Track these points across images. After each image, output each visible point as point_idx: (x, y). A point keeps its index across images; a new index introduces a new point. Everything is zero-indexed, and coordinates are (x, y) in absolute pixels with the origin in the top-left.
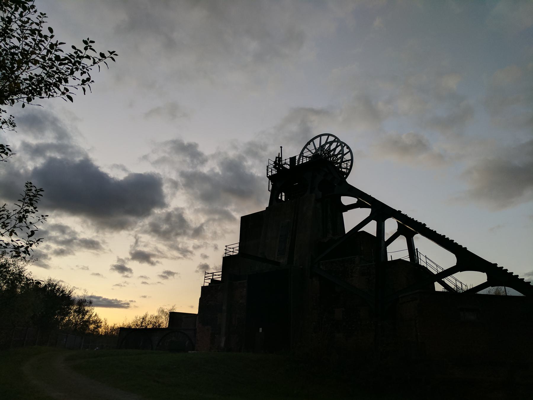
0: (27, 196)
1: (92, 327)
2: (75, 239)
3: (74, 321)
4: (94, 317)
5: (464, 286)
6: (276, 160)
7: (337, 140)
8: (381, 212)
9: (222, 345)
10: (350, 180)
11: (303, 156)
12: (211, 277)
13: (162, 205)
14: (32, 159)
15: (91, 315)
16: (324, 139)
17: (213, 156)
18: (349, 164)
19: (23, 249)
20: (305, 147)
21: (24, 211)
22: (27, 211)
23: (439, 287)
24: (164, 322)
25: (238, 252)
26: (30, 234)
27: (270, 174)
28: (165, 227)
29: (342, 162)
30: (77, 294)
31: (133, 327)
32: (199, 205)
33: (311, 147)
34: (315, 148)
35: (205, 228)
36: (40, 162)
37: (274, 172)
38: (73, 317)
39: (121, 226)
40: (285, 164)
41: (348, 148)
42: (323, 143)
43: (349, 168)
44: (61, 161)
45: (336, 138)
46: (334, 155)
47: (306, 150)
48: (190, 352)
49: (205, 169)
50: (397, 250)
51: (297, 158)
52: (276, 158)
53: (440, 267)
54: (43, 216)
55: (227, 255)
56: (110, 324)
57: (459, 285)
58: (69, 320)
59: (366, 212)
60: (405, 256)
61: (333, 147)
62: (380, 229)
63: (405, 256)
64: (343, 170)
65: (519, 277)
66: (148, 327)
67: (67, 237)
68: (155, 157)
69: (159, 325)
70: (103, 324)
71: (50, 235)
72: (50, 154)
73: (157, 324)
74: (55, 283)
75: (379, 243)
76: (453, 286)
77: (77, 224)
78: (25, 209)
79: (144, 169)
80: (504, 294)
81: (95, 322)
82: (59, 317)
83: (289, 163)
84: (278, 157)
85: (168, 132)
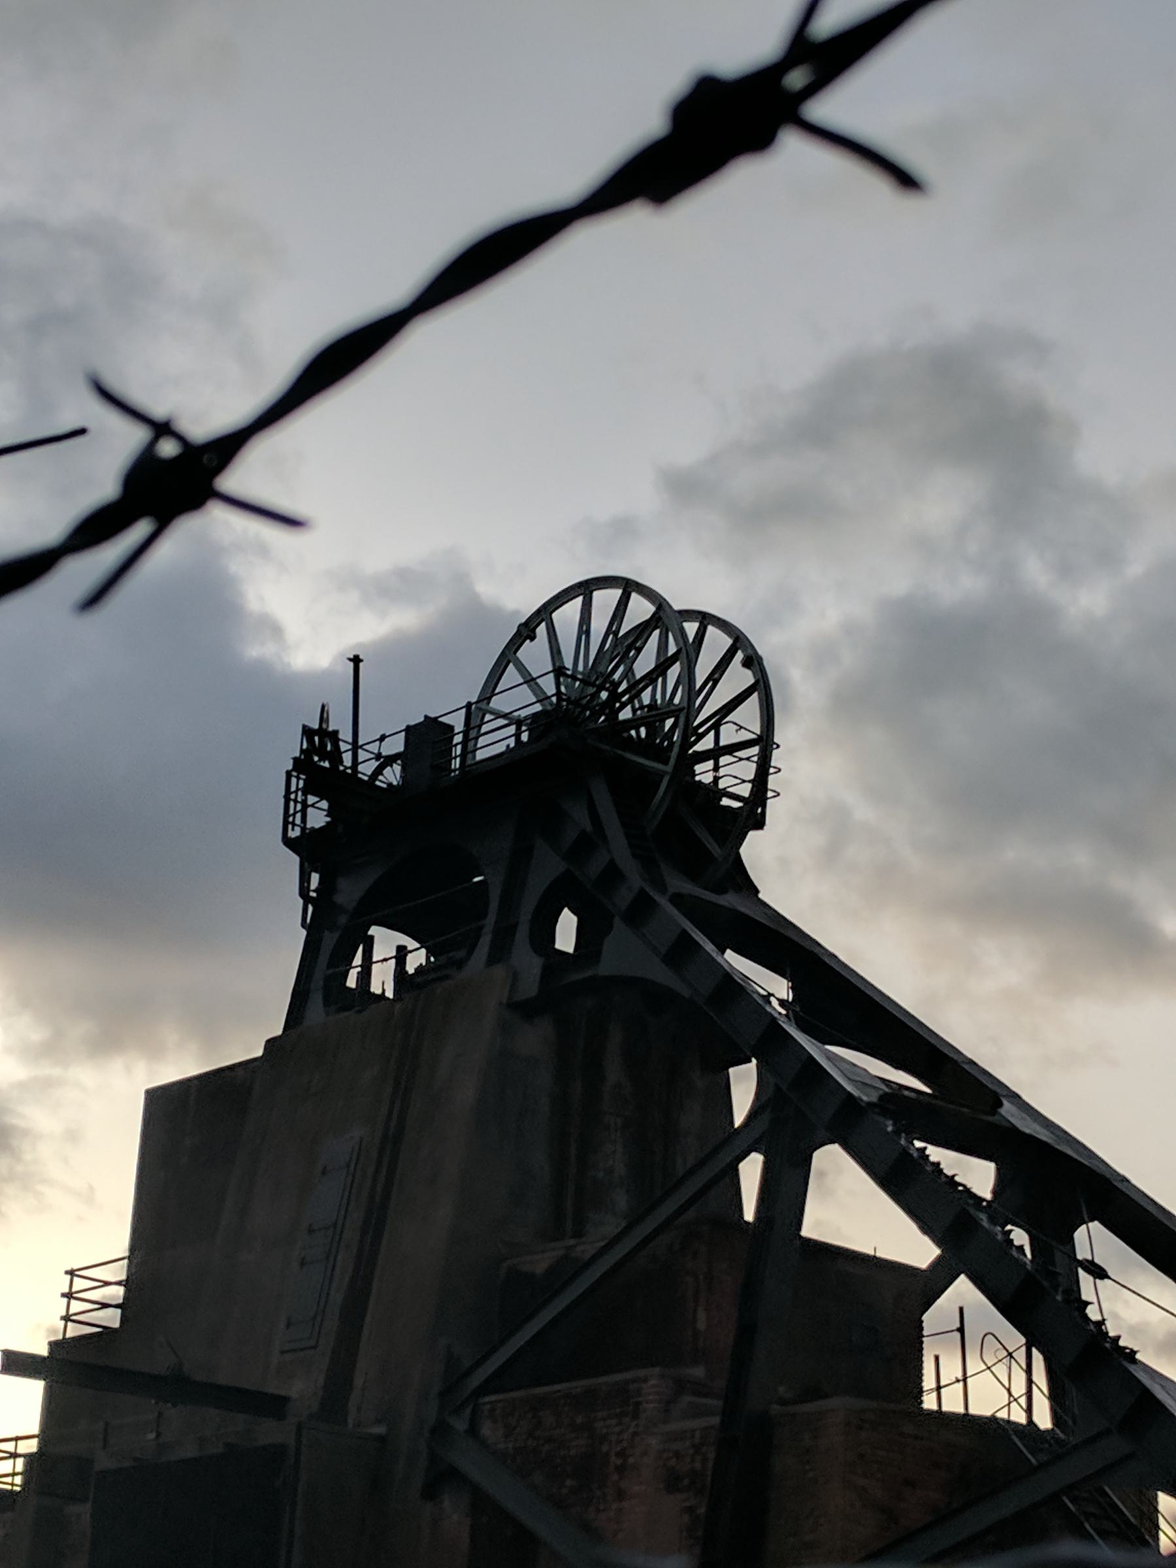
18: (749, 770)
27: (294, 833)
33: (536, 654)
47: (511, 675)
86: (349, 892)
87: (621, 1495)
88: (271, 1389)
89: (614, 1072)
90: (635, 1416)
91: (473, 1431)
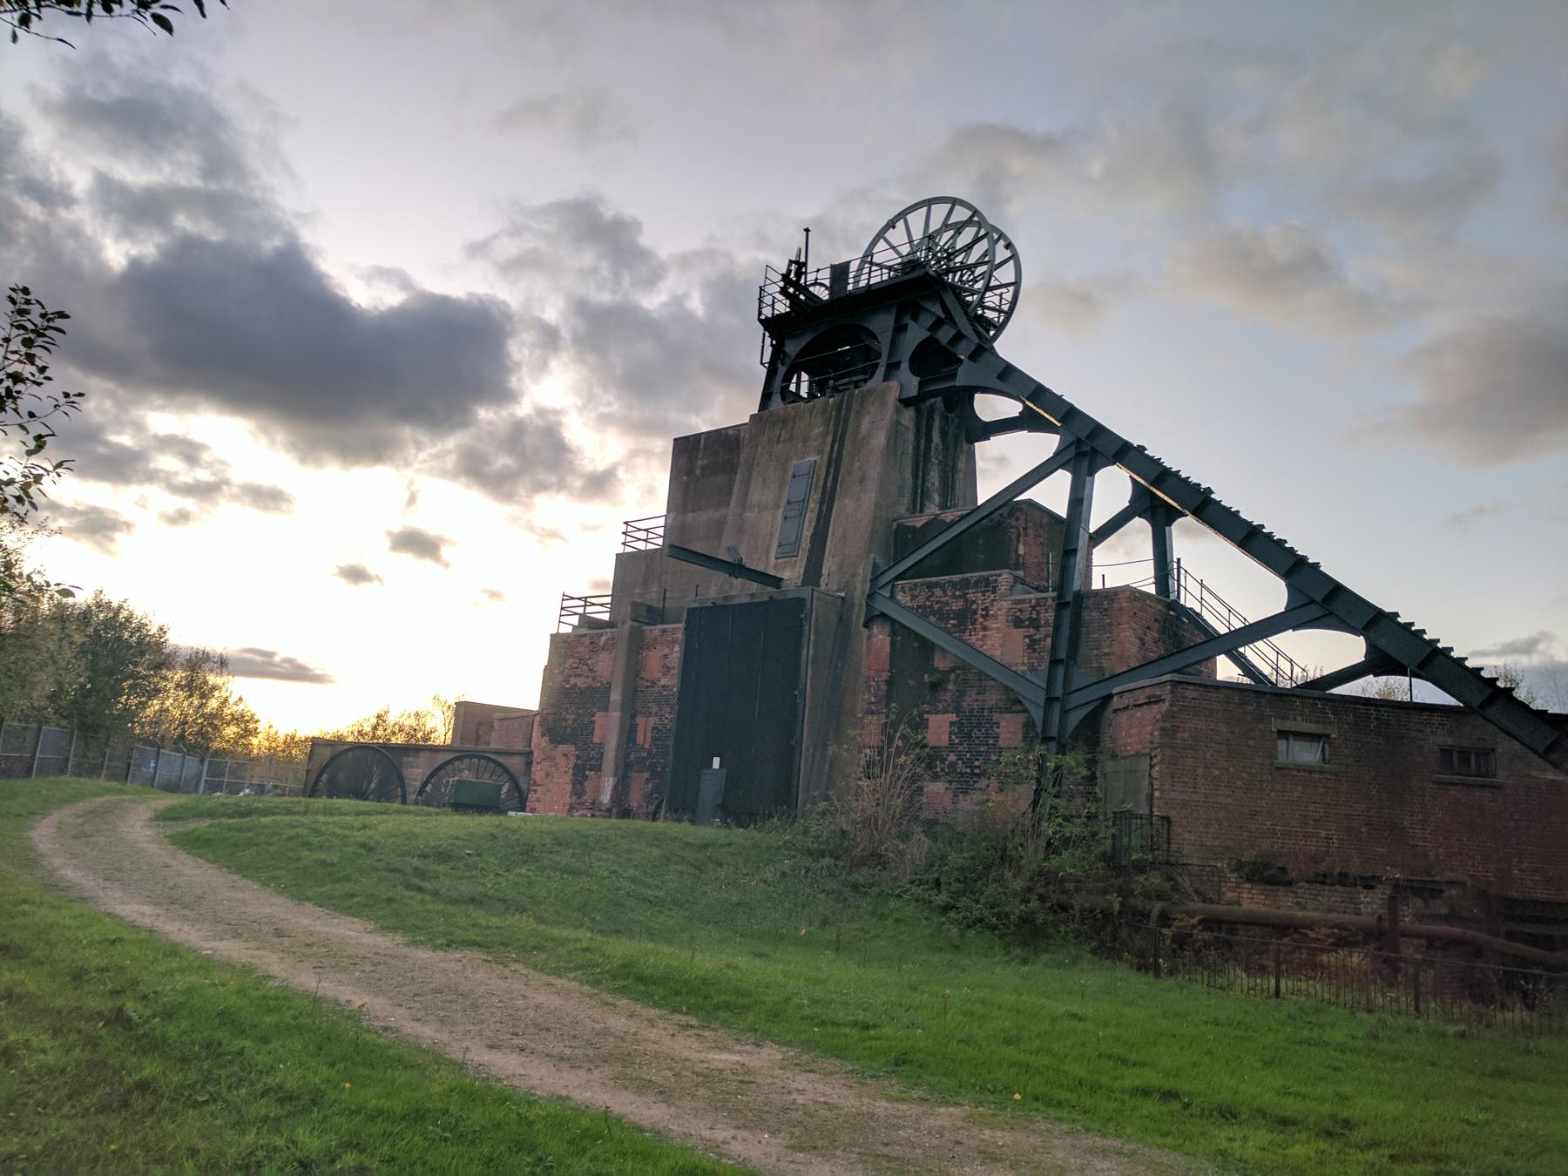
0: (15, 332)
1: (231, 731)
2: (227, 482)
3: (177, 713)
4: (236, 704)
5: (1297, 672)
6: (789, 271)
7: (976, 219)
8: (1087, 446)
9: (606, 798)
10: (1007, 347)
11: (871, 263)
12: (580, 610)
13: (503, 395)
14: (125, 233)
15: (226, 700)
16: (939, 212)
17: (685, 261)
18: (1008, 296)
19: (12, 491)
20: (880, 235)
21: (9, 376)
22: (17, 378)
23: (1226, 670)
24: (441, 730)
25: (660, 541)
26: (32, 445)
27: (767, 312)
28: (503, 461)
29: (988, 288)
30: (183, 637)
31: (350, 739)
32: (612, 403)
33: (897, 236)
34: (911, 242)
35: (621, 473)
36: (150, 247)
37: (782, 307)
38: (172, 703)
39: (376, 451)
40: (816, 283)
41: (1009, 246)
42: (935, 225)
43: (1005, 308)
44: (219, 251)
45: (975, 212)
46: (964, 267)
47: (882, 245)
48: (512, 813)
49: (653, 302)
50: (1120, 565)
51: (854, 267)
52: (791, 262)
53: (1237, 614)
54: (67, 395)
55: (628, 550)
56: (283, 730)
57: (1285, 666)
58: (164, 711)
59: (1045, 444)
60: (1142, 577)
61: (961, 242)
62: (1079, 501)
63: (1142, 577)
64: (989, 314)
65: (1454, 654)
66: (394, 740)
67: (203, 475)
68: (509, 248)
69: (426, 738)
70: (261, 727)
71: (152, 465)
72: (183, 222)
73: (419, 735)
74: (115, 605)
75: (1068, 537)
76: (1266, 670)
77: (233, 438)
78: (10, 370)
79: (463, 283)
80: (1407, 698)
81: (238, 719)
82: (134, 701)
83: (827, 283)
84: (797, 262)
85: (554, 173)
86: (792, 348)
87: (985, 629)
88: (772, 572)
89: (936, 439)
90: (994, 592)
91: (892, 597)
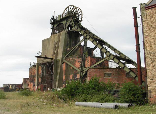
33: (66, 11)
